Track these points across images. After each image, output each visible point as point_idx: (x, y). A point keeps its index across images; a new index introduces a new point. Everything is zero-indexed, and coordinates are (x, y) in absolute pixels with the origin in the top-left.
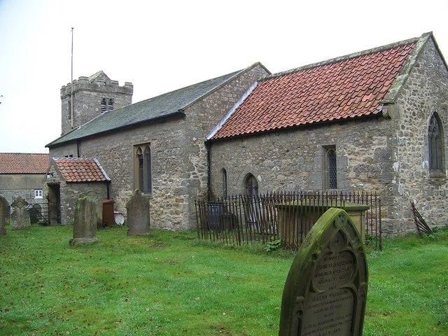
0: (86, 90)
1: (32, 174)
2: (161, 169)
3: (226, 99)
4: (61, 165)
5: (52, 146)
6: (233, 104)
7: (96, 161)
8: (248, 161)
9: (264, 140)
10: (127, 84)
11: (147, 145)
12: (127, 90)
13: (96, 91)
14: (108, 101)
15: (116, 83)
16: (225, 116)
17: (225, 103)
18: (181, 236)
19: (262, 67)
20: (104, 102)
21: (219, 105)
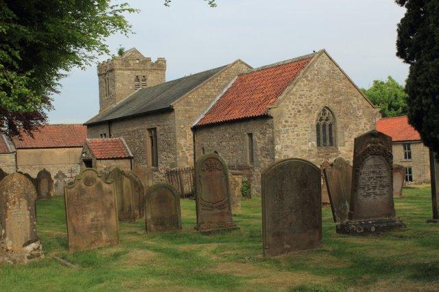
0: (120, 69)
1: (75, 147)
2: (163, 148)
3: (209, 93)
4: (92, 145)
5: (91, 125)
6: (215, 97)
7: (123, 140)
8: (215, 143)
9: (222, 128)
10: (160, 59)
11: (155, 129)
12: (160, 65)
13: (129, 70)
14: (141, 78)
15: (149, 59)
16: (208, 106)
17: (209, 96)
18: (397, 143)
19: (242, 63)
20: (137, 79)
21: (203, 99)
